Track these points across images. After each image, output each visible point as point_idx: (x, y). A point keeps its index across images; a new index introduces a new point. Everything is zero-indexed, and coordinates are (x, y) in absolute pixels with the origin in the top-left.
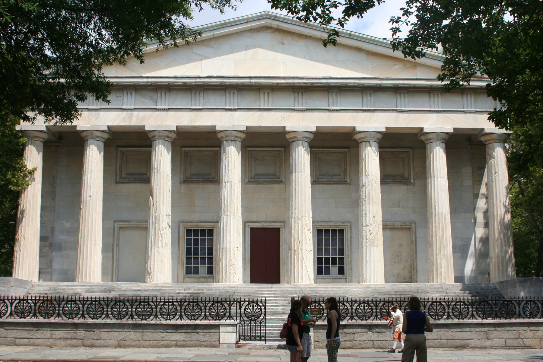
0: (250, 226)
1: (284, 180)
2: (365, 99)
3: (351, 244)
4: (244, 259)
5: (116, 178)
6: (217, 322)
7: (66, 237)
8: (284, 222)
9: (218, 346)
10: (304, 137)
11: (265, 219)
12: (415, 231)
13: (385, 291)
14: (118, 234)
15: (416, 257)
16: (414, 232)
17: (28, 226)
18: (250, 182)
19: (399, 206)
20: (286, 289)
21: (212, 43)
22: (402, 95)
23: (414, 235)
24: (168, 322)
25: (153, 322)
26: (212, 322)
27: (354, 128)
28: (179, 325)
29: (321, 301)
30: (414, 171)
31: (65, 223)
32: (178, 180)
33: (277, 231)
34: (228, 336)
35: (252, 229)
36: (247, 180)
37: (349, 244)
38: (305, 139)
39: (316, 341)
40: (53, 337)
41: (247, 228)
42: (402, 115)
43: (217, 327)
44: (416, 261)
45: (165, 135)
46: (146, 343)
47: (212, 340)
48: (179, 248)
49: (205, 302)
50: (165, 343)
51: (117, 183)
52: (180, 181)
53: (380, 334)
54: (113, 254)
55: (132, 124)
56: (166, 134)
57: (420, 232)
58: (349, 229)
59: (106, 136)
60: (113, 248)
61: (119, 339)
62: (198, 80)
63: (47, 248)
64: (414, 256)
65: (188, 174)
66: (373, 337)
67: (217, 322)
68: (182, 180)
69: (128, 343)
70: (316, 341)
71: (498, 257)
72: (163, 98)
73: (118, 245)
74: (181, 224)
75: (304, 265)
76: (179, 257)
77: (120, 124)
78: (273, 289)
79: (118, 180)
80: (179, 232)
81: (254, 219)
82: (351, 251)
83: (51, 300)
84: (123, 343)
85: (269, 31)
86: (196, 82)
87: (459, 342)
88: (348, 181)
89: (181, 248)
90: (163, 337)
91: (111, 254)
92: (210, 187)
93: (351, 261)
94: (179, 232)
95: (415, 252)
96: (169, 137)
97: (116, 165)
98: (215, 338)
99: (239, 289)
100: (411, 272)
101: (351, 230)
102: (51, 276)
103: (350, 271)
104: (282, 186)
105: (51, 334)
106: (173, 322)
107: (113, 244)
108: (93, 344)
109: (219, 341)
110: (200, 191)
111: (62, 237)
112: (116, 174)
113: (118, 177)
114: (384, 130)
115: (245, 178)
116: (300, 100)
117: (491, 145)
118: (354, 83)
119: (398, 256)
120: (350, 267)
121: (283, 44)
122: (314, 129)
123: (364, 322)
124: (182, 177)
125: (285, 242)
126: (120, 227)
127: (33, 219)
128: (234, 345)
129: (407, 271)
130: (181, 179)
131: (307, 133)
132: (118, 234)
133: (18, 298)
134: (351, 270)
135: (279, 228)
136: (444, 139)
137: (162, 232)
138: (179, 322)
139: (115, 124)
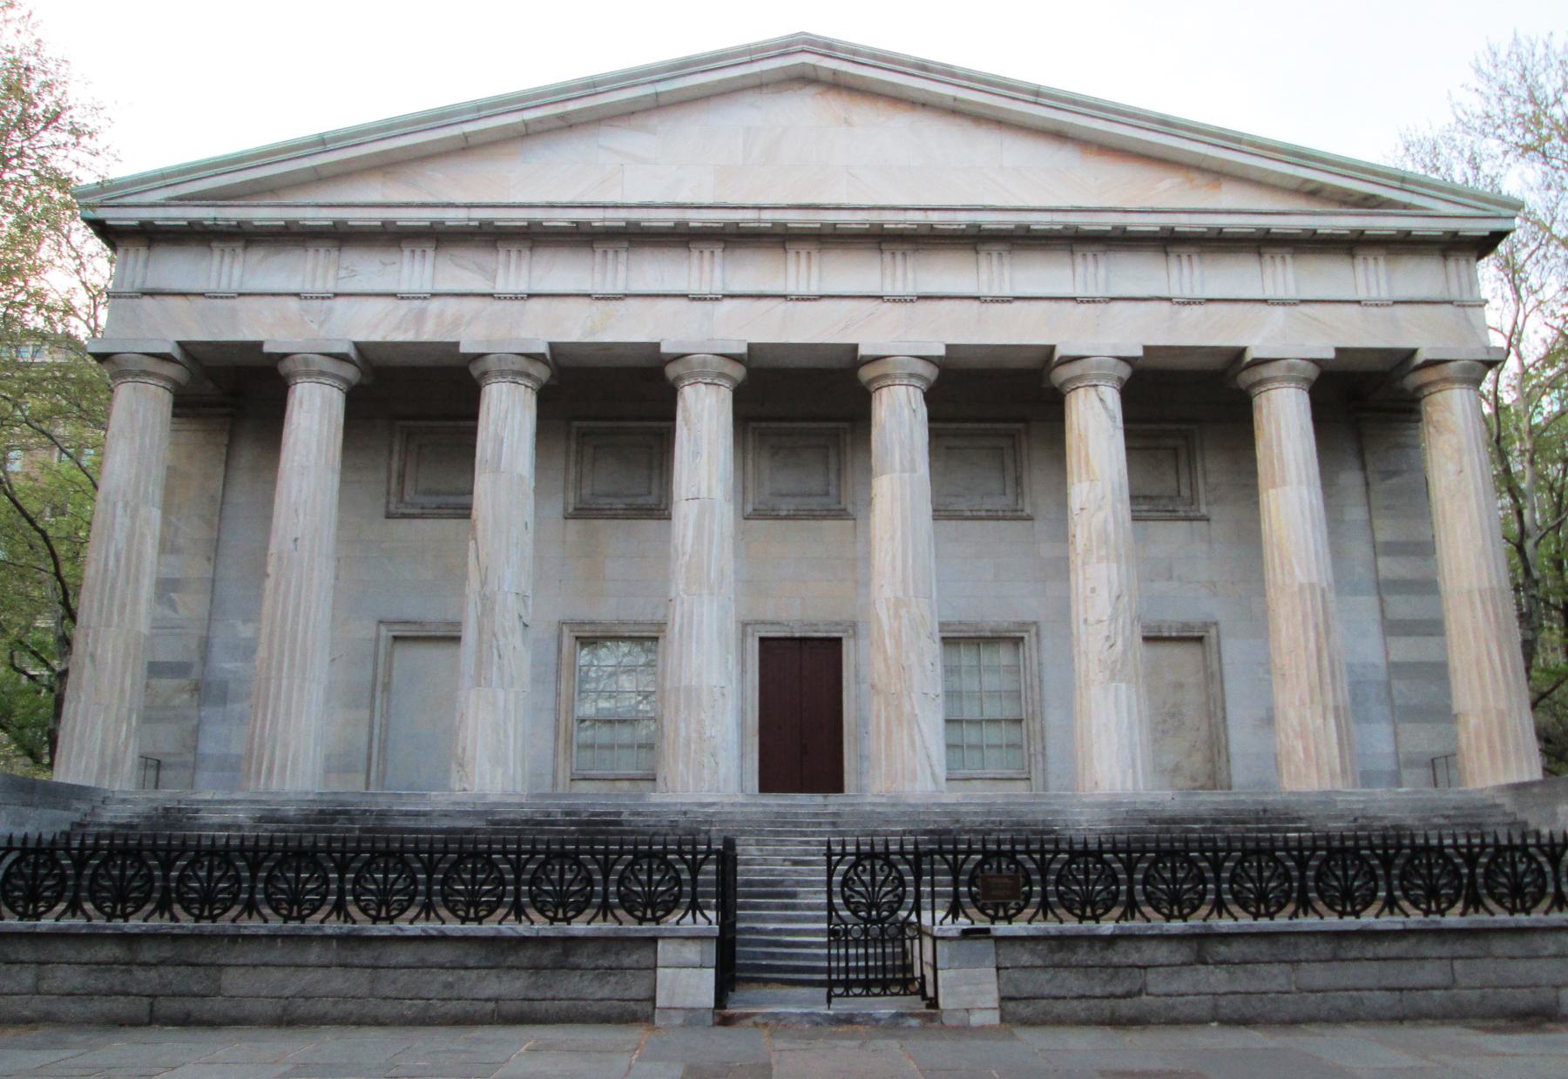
0: (758, 635)
1: (850, 509)
2: (1080, 269)
3: (1041, 681)
4: (742, 724)
5: (388, 503)
6: (648, 928)
7: (239, 664)
8: (854, 625)
9: (648, 1019)
10: (911, 375)
11: (798, 613)
12: (1219, 644)
13: (1167, 814)
14: (389, 655)
15: (1224, 718)
16: (1215, 649)
17: (108, 625)
18: (759, 514)
19: (1170, 578)
20: (868, 808)
21: (654, 120)
22: (707, 254)
23: (1215, 657)
24: (471, 928)
25: (418, 928)
26: (631, 927)
27: (1051, 349)
28: (510, 939)
29: (893, 848)
30: (1206, 483)
31: (240, 627)
32: (555, 508)
33: (832, 646)
34: (686, 980)
35: (762, 640)
36: (749, 509)
37: (1036, 682)
38: (914, 381)
39: (1011, 999)
40: (45, 986)
41: (749, 640)
42: (1187, 311)
43: (654, 940)
44: (1225, 728)
45: (516, 367)
46: (387, 1009)
47: (627, 995)
48: (558, 694)
49: (343, 853)
50: (455, 1007)
51: (389, 516)
52: (565, 509)
53: (1239, 970)
54: (373, 711)
55: (424, 338)
56: (521, 364)
57: (1234, 650)
58: (1034, 639)
59: (350, 372)
60: (373, 697)
61: (287, 993)
62: (610, 214)
63: (186, 696)
64: (1220, 714)
65: (586, 491)
66: (1212, 979)
67: (648, 928)
68: (570, 510)
69: (322, 1007)
70: (1011, 999)
71: (1485, 711)
72: (513, 267)
73: (387, 687)
74: (565, 629)
75: (917, 737)
76: (557, 720)
77: (389, 339)
78: (831, 809)
79: (392, 508)
80: (560, 650)
81: (769, 617)
82: (1041, 700)
83: (1101, 851)
84: (302, 1008)
85: (810, 91)
86: (604, 220)
87: (1524, 999)
88: (1028, 510)
89: (563, 697)
90: (449, 986)
91: (366, 714)
92: (650, 526)
93: (1042, 728)
94: (560, 650)
95: (1219, 704)
96: (528, 376)
97: (390, 465)
98: (638, 989)
99: (727, 809)
100: (1211, 760)
101: (1038, 641)
102: (193, 776)
103: (1040, 757)
104: (851, 523)
105: (39, 978)
106: (489, 927)
107: (374, 685)
108: (188, 1015)
109: (653, 999)
110: (616, 537)
111: (227, 666)
112: (388, 493)
113: (393, 500)
114: (1140, 353)
115: (744, 501)
116: (899, 273)
117: (1438, 397)
118: (1052, 223)
119: (1173, 715)
120: (1039, 747)
121: (847, 122)
122: (941, 352)
123: (1177, 926)
124: (571, 499)
125: (857, 676)
126: (396, 638)
127: (123, 606)
128: (709, 1018)
129: (1198, 758)
130: (566, 504)
131: (920, 363)
132: (389, 655)
133: (17, 844)
134: (1044, 755)
135: (839, 640)
136: (1305, 379)
137: (502, 641)
138: (512, 927)
139: (376, 337)
